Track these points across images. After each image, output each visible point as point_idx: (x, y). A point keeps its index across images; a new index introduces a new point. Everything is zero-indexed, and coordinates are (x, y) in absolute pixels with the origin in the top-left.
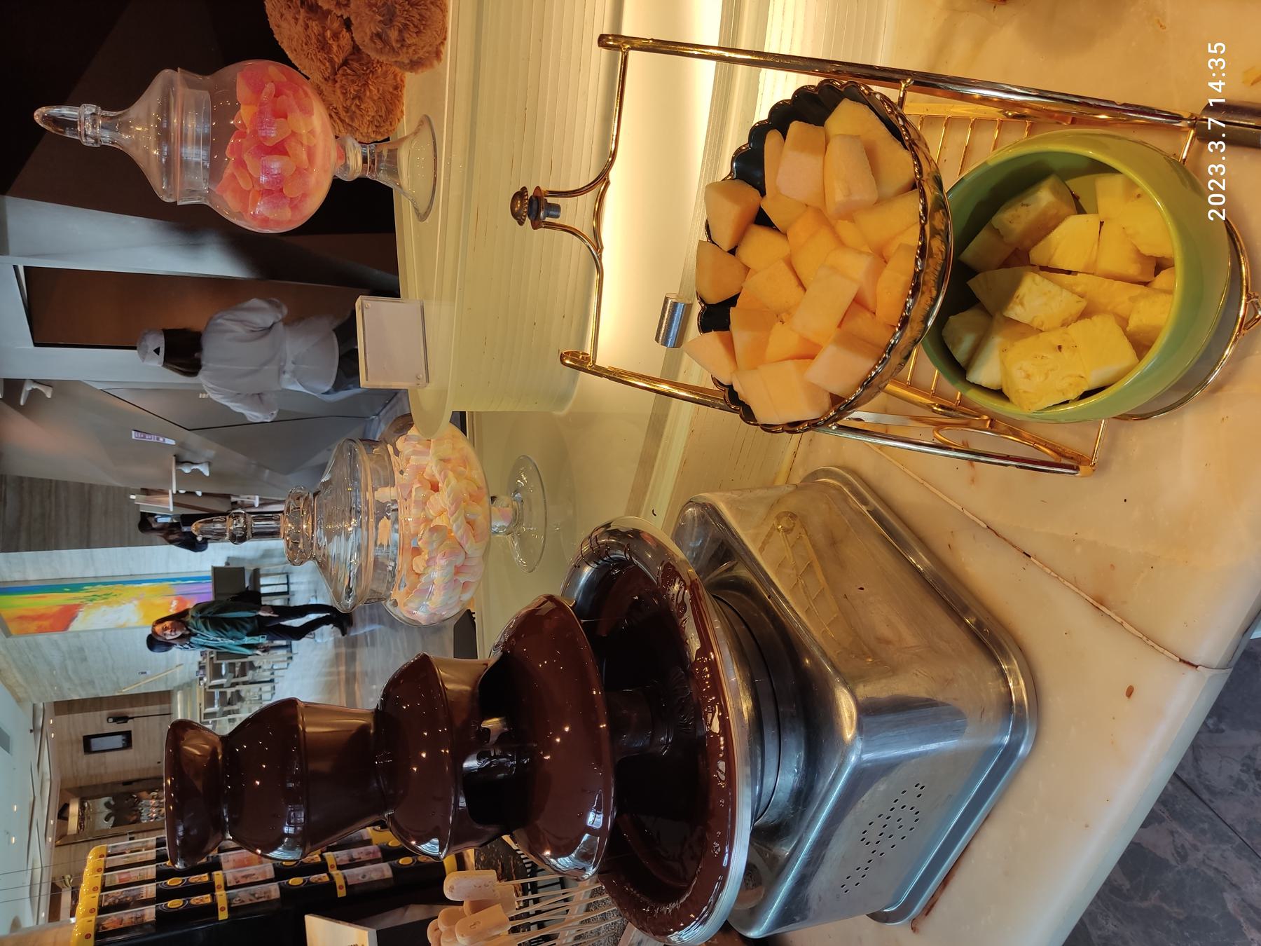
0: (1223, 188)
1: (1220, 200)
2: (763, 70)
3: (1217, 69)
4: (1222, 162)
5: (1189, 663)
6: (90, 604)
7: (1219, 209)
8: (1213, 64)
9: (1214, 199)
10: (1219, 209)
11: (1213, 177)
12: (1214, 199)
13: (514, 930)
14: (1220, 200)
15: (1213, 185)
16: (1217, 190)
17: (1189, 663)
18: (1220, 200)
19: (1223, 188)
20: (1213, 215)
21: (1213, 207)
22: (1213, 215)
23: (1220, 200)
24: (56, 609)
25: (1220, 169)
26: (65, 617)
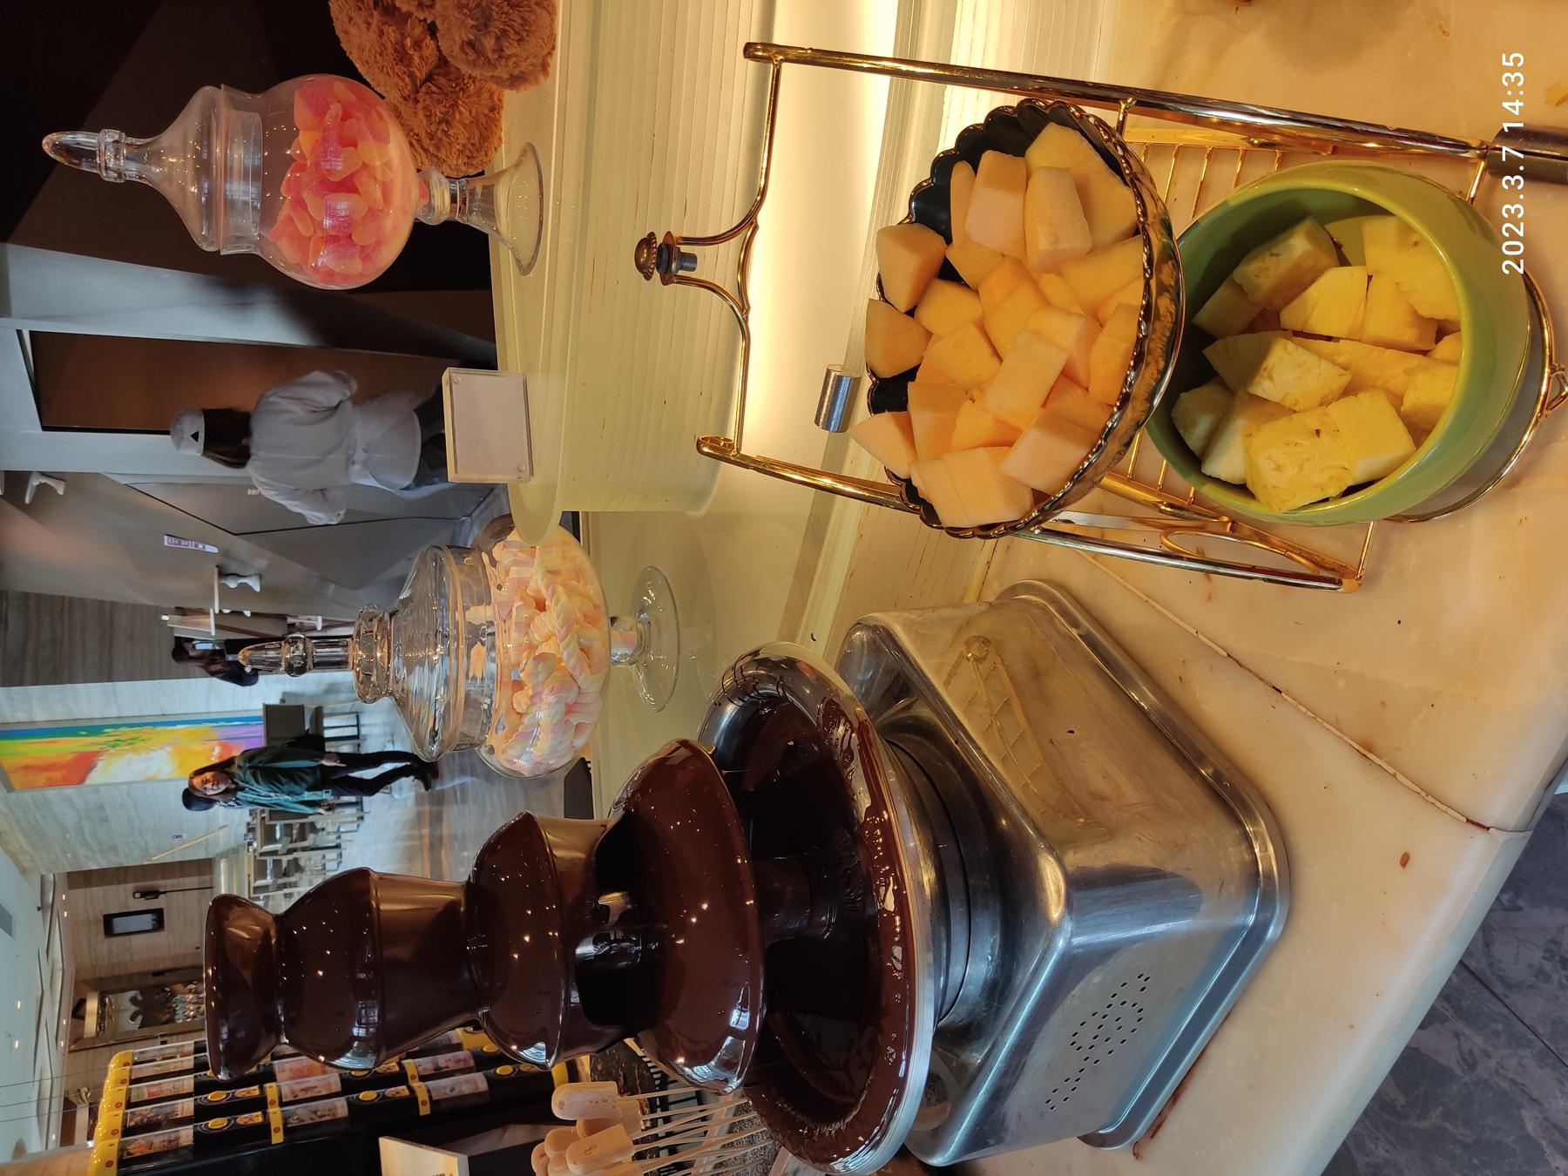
0: (1521, 234)
1: (1517, 248)
2: (949, 87)
3: (1513, 85)
4: (1520, 202)
5: (1478, 825)
6: (112, 751)
7: (1516, 260)
8: (1508, 79)
9: (1510, 248)
10: (1516, 260)
11: (1508, 221)
12: (1510, 248)
13: (640, 1156)
14: (1517, 248)
15: (1508, 230)
16: (1514, 236)
17: (1478, 825)
18: (1517, 248)
19: (1521, 234)
20: (1508, 267)
21: (1508, 258)
22: (1508, 267)
23: (1517, 248)
24: (69, 757)
25: (1518, 211)
26: (81, 767)
